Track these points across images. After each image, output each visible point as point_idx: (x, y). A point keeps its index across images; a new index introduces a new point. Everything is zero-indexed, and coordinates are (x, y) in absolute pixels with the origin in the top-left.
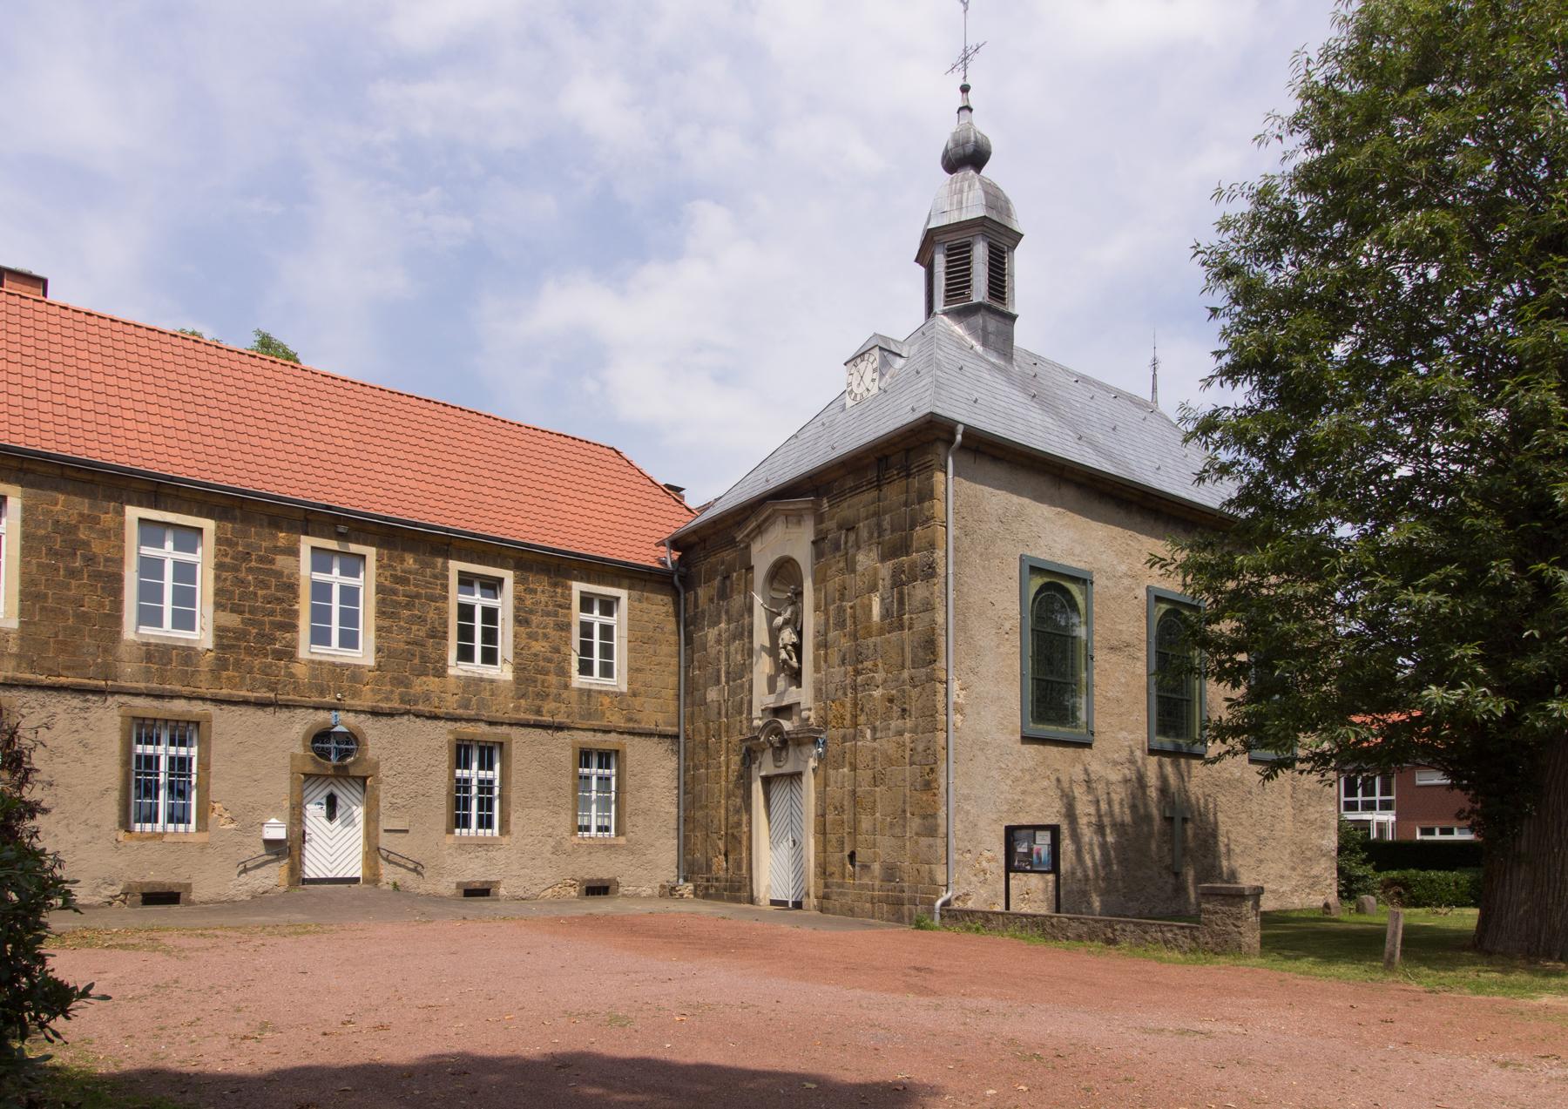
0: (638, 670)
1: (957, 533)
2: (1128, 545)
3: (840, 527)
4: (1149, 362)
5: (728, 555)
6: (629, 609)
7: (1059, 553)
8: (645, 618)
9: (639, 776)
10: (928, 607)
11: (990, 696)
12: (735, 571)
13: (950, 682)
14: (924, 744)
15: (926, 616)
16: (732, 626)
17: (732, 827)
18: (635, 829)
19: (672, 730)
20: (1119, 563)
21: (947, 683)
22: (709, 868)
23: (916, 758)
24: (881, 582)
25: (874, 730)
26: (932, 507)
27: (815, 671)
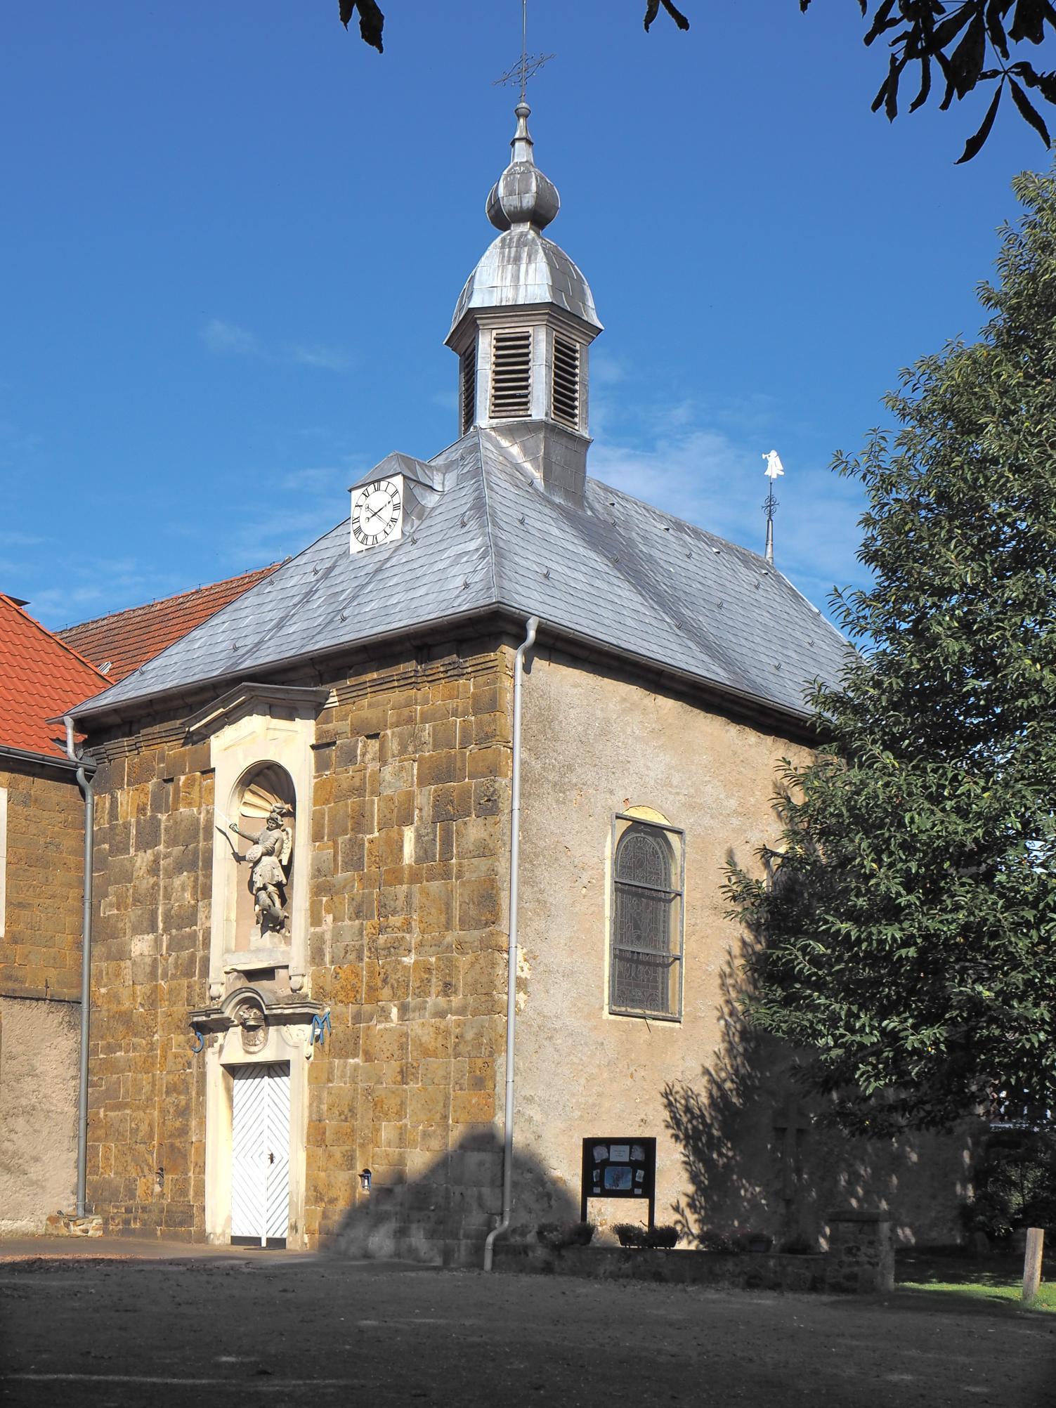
0: (21, 905)
1: (525, 755)
2: (740, 773)
3: (356, 732)
5: (170, 749)
7: (652, 783)
10: (485, 851)
12: (184, 773)
13: (513, 950)
14: (475, 1030)
15: (483, 864)
18: (13, 1136)
19: (67, 993)
21: (508, 953)
22: (131, 1193)
23: (462, 1048)
24: (417, 812)
25: (404, 1009)
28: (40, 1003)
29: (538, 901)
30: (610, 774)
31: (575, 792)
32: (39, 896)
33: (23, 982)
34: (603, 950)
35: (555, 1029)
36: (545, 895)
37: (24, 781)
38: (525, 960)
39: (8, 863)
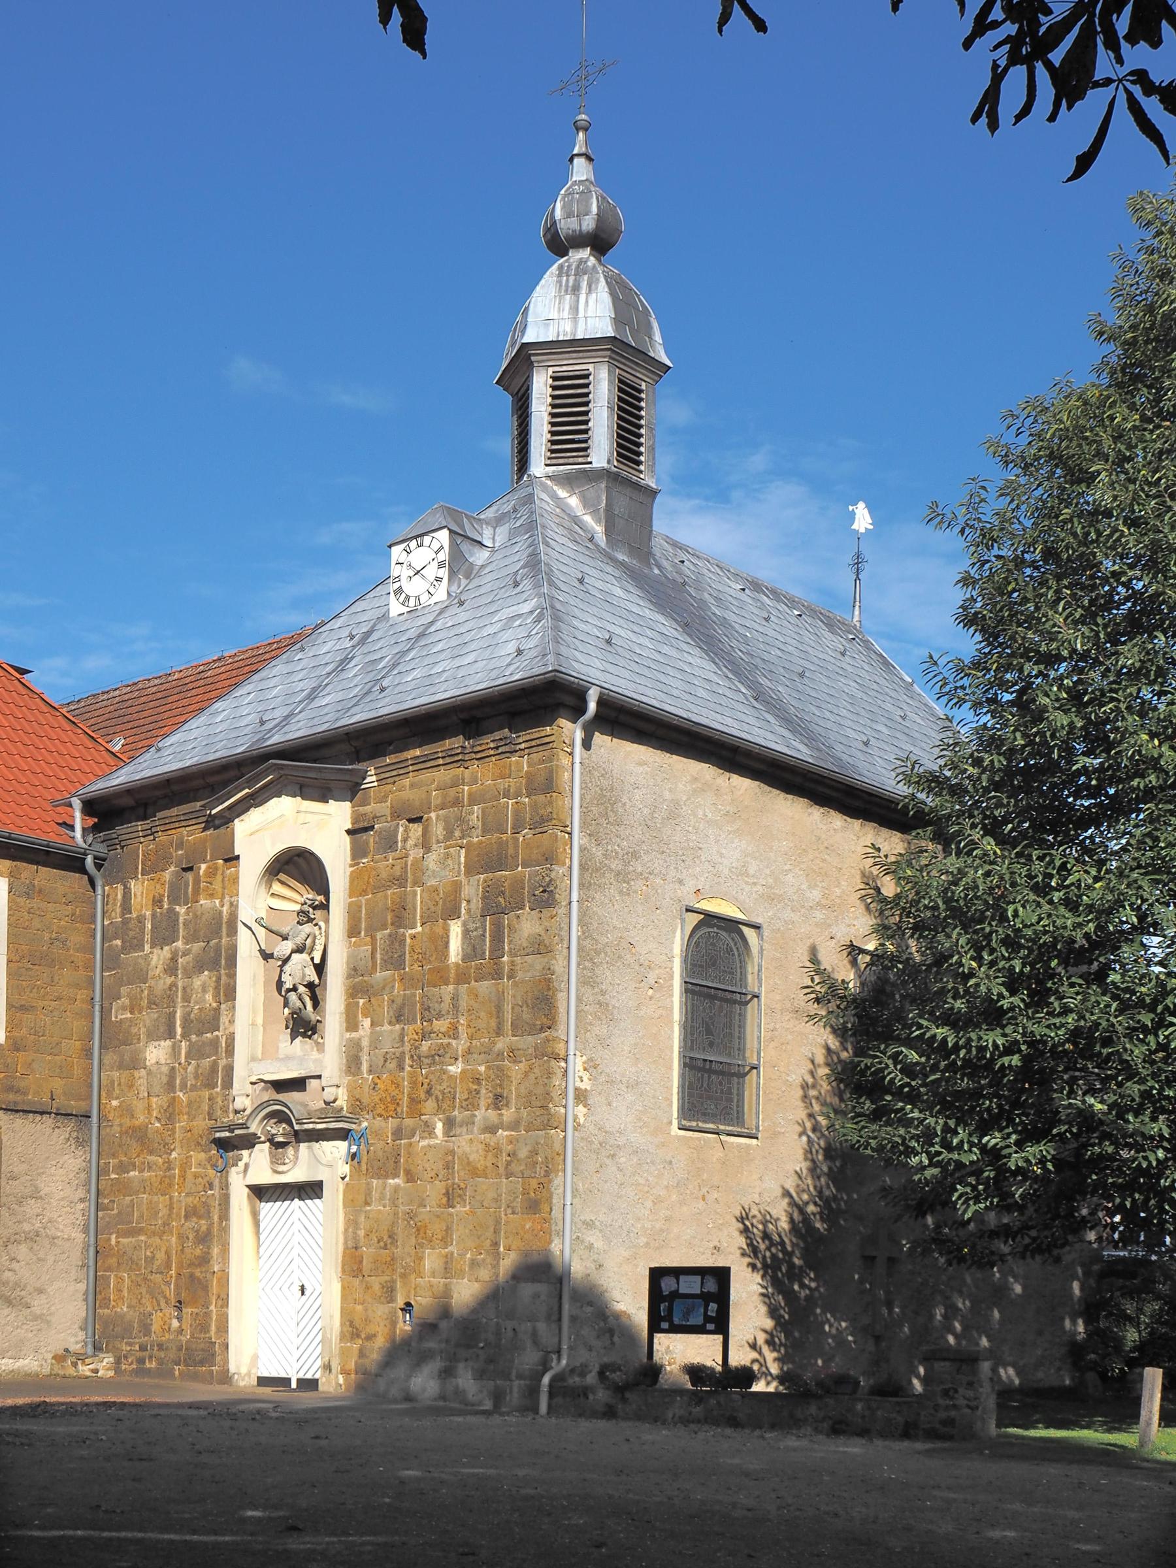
0: (23, 1008)
2: (824, 860)
3: (396, 815)
4: (849, 558)
6: (10, 909)
7: (726, 871)
8: (36, 923)
9: (23, 1179)
10: (540, 948)
11: (624, 1080)
12: (204, 861)
14: (529, 1148)
15: (538, 962)
16: (197, 947)
17: (191, 1265)
18: (14, 1265)
19: (75, 1106)
20: (810, 887)
21: (566, 1061)
23: (514, 1167)
24: (464, 904)
25: (450, 1124)
26: (551, 803)
27: (347, 1030)
28: (45, 1117)
29: (600, 1004)
30: (679, 862)
31: (640, 883)
32: (43, 998)
33: (25, 1094)
34: (671, 1059)
35: (618, 1146)
36: (607, 996)
37: (27, 870)
38: (585, 1069)
39: (9, 961)
